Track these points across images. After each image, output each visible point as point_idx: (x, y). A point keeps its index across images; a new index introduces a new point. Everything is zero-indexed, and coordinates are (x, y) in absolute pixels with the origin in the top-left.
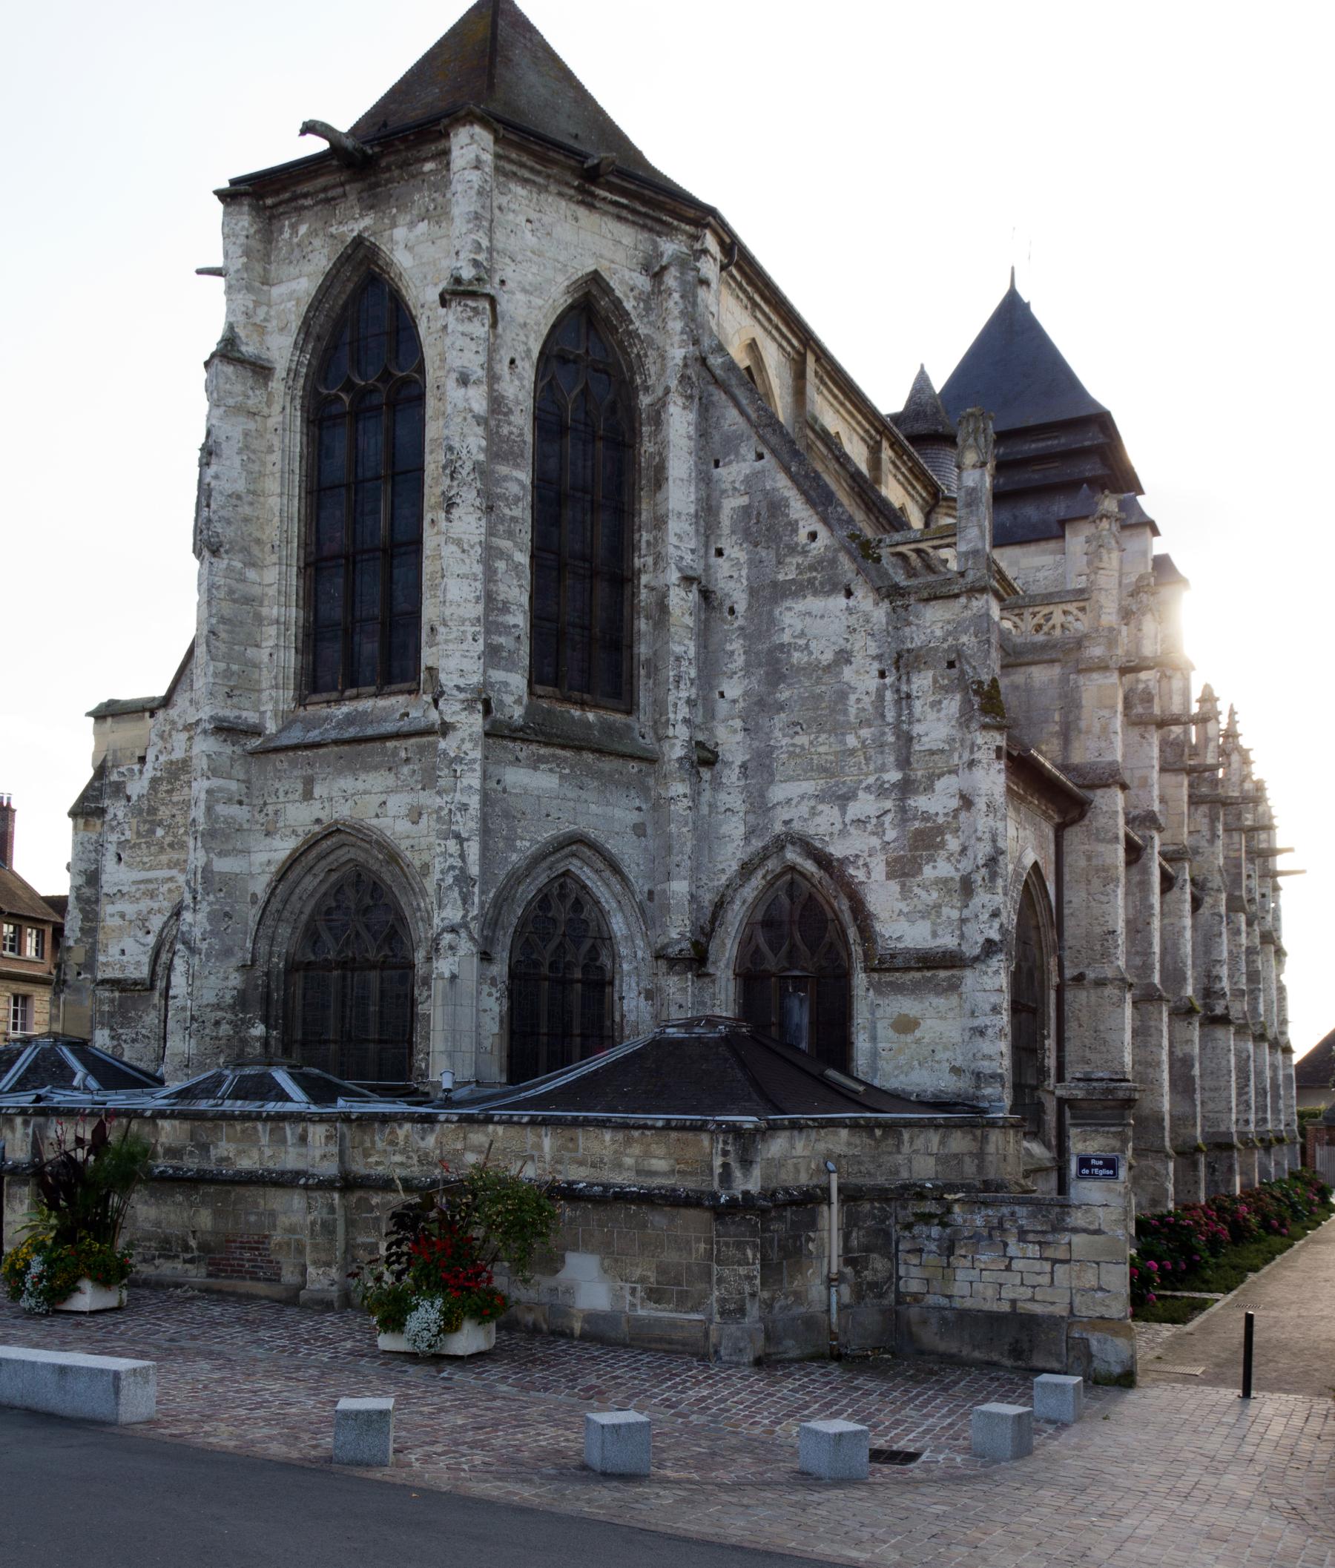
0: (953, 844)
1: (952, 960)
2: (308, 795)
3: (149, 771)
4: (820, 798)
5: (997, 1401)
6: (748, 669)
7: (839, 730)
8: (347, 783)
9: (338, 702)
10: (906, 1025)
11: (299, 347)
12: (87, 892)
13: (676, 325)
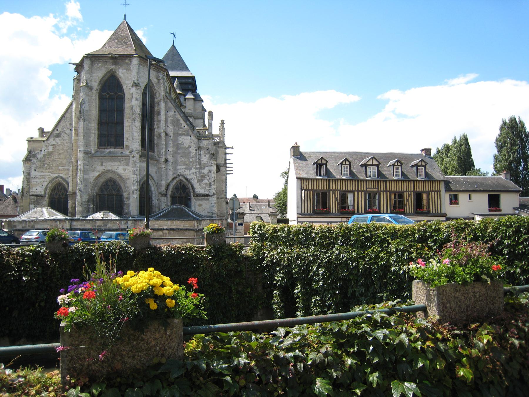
0: (208, 178)
1: (208, 195)
2: (102, 165)
3: (43, 153)
4: (186, 169)
5: (411, 184)
6: (173, 146)
7: (189, 158)
8: (110, 163)
9: (107, 148)
10: (200, 205)
11: (98, 85)
12: (28, 177)
13: (162, 89)
